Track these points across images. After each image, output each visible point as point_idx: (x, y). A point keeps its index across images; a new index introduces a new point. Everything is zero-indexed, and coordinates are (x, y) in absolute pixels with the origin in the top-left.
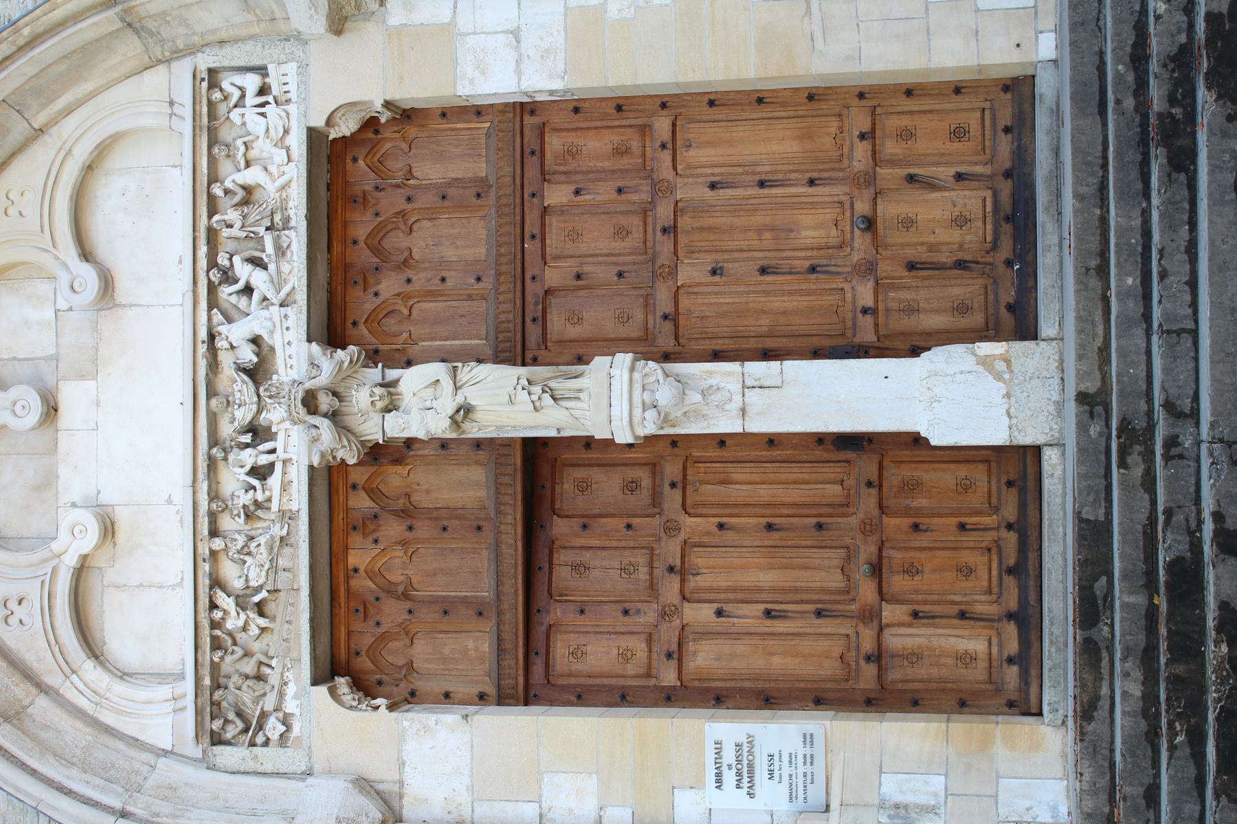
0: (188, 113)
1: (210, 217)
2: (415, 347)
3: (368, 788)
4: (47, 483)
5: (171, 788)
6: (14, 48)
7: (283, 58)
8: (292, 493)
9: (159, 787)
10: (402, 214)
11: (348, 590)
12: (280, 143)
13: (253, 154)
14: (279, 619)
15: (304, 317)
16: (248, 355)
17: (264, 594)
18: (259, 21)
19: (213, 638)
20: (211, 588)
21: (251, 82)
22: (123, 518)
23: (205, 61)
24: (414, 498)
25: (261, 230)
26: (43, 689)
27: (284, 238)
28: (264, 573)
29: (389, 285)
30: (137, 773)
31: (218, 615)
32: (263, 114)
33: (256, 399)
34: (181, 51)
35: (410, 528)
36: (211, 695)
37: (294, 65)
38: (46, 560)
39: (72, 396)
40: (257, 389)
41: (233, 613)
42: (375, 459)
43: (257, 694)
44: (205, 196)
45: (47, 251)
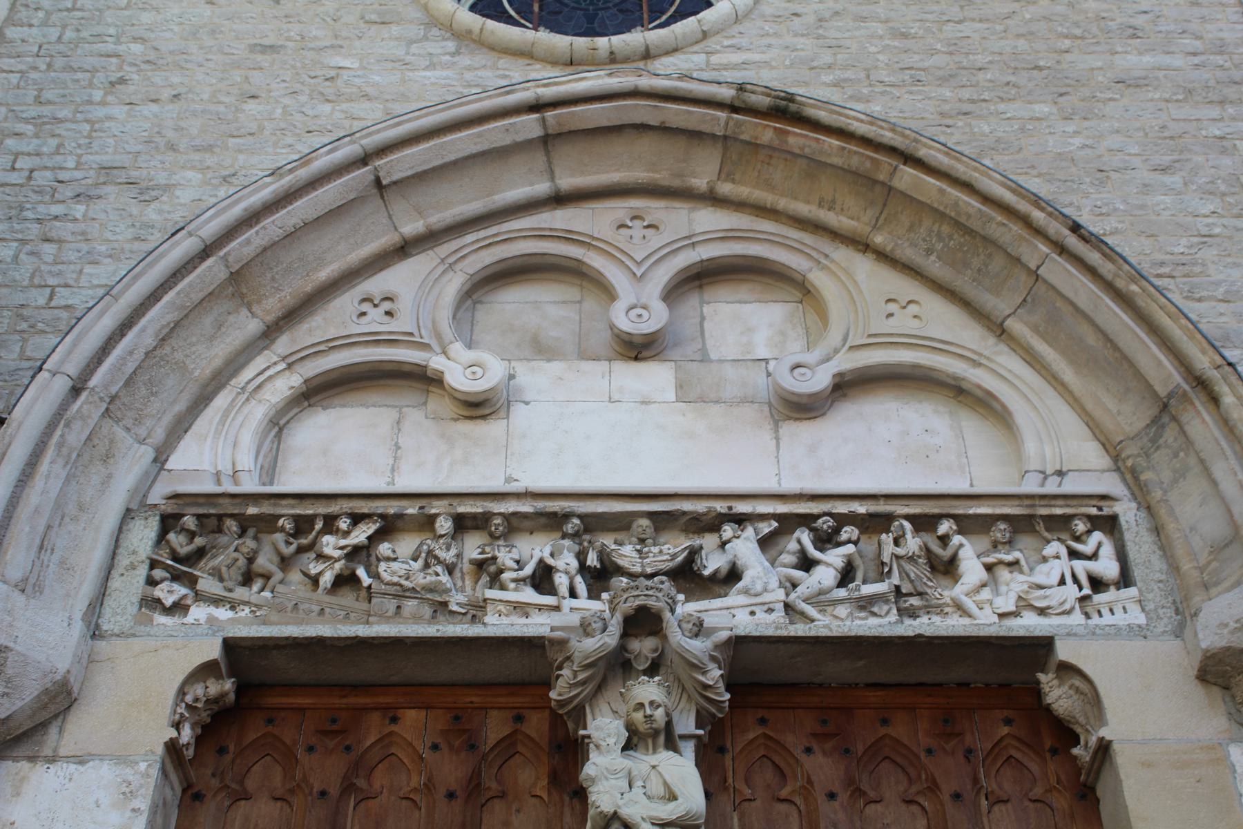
0: (1051, 487)
1: (907, 517)
2: (729, 808)
3: (53, 709)
4: (542, 349)
5: (107, 458)
6: (1109, 277)
7: (1151, 606)
8: (511, 615)
9: (111, 441)
10: (933, 787)
11: (365, 709)
12: (1025, 603)
13: (1004, 574)
14: (328, 598)
15: (770, 632)
16: (713, 563)
17: (366, 580)
18: (1201, 570)
19: (310, 518)
20: (383, 516)
21: (1107, 567)
22: (492, 429)
23: (1127, 511)
24: (498, 805)
25: (895, 580)
26: (271, 332)
27: (886, 608)
28: (395, 579)
29: (823, 768)
30: (138, 421)
31: (343, 524)
32: (1062, 582)
33: (649, 570)
34: (1136, 479)
35: (451, 795)
36: (232, 516)
37: (1141, 619)
38: (438, 336)
39: (655, 377)
40: (664, 574)
41: (343, 542)
42: (559, 747)
43: (224, 569)
44: (936, 511)
45: (845, 339)
